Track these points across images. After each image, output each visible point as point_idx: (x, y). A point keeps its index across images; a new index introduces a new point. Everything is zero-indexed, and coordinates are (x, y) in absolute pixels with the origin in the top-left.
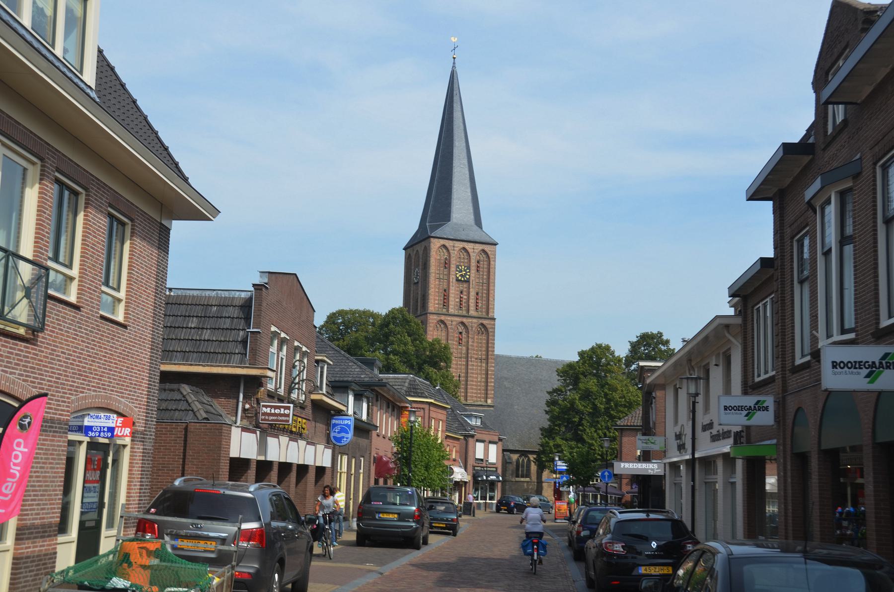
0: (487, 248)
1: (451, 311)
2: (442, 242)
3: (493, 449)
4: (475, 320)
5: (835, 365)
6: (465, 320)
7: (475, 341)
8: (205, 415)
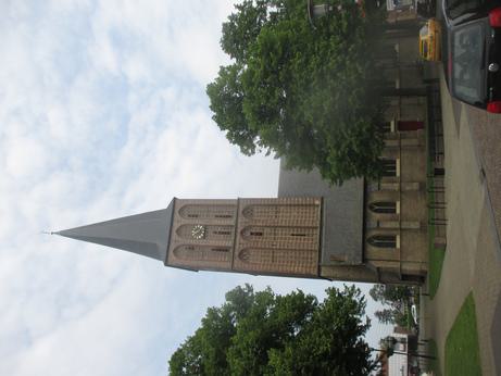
1: (230, 244)
6: (239, 231)
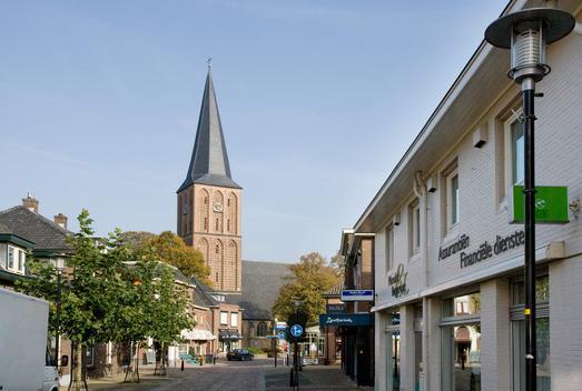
0: (235, 191)
1: (211, 232)
3: (234, 316)
7: (228, 252)
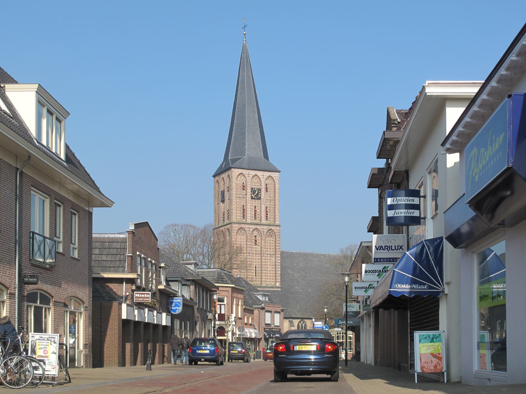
2: (240, 171)
3: (277, 316)
4: (265, 227)
5: (355, 288)
8: (109, 299)
